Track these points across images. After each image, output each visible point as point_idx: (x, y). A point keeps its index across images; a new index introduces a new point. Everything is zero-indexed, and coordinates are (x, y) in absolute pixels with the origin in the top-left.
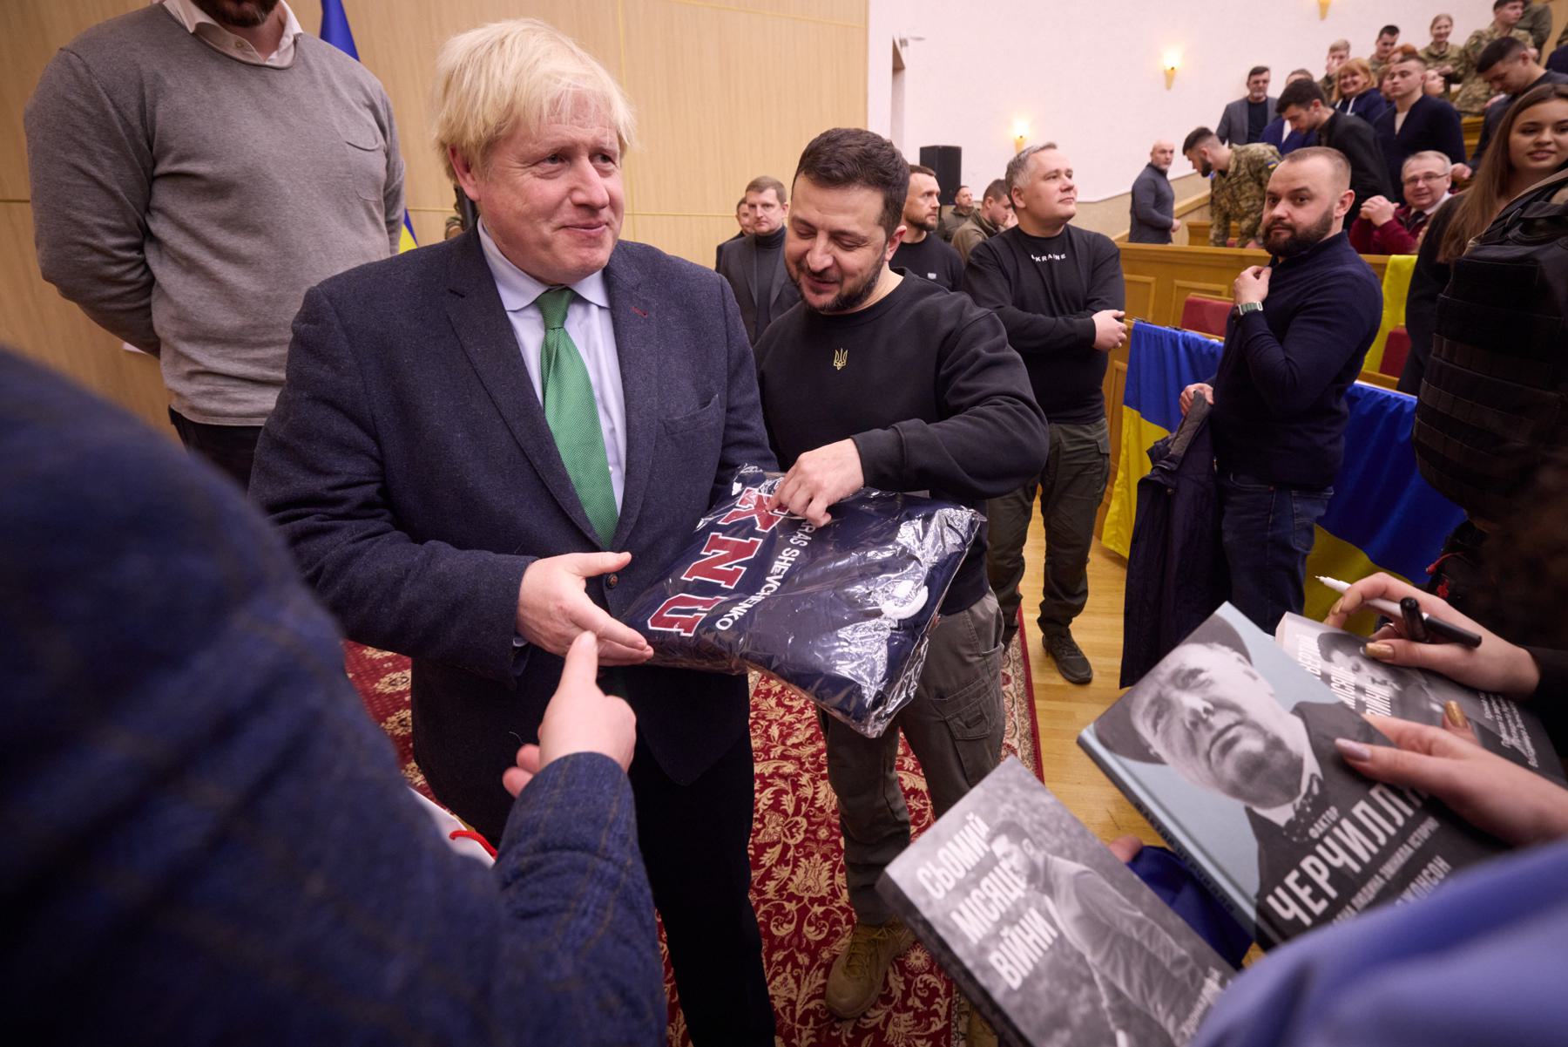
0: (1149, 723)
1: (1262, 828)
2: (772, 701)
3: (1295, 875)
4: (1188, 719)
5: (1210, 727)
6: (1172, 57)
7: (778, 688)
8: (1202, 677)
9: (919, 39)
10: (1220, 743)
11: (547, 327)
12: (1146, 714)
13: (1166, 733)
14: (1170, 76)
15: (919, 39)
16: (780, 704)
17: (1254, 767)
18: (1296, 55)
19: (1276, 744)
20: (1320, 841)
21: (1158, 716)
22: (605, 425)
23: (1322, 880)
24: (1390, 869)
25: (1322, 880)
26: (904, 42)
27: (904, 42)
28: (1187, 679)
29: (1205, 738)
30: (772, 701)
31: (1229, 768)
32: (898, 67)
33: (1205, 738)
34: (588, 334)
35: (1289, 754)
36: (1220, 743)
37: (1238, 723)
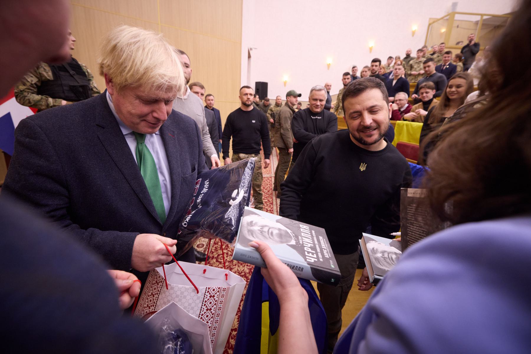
0: (251, 237)
1: (292, 246)
2: (215, 260)
3: (306, 253)
4: (259, 232)
5: (265, 232)
6: (329, 60)
7: (216, 256)
8: (254, 222)
9: (256, 49)
10: (270, 234)
11: (138, 144)
12: (249, 235)
13: (257, 237)
14: (329, 66)
15: (256, 49)
16: (217, 261)
17: (280, 236)
18: (361, 63)
19: (279, 230)
20: (303, 244)
21: (252, 234)
22: (161, 178)
23: (310, 250)
24: (316, 242)
25: (310, 250)
26: (251, 49)
27: (251, 49)
28: (251, 224)
29: (266, 234)
30: (215, 260)
31: (276, 238)
32: (249, 57)
33: (266, 234)
34: (153, 144)
35: (284, 230)
36: (270, 234)
37: (269, 229)
